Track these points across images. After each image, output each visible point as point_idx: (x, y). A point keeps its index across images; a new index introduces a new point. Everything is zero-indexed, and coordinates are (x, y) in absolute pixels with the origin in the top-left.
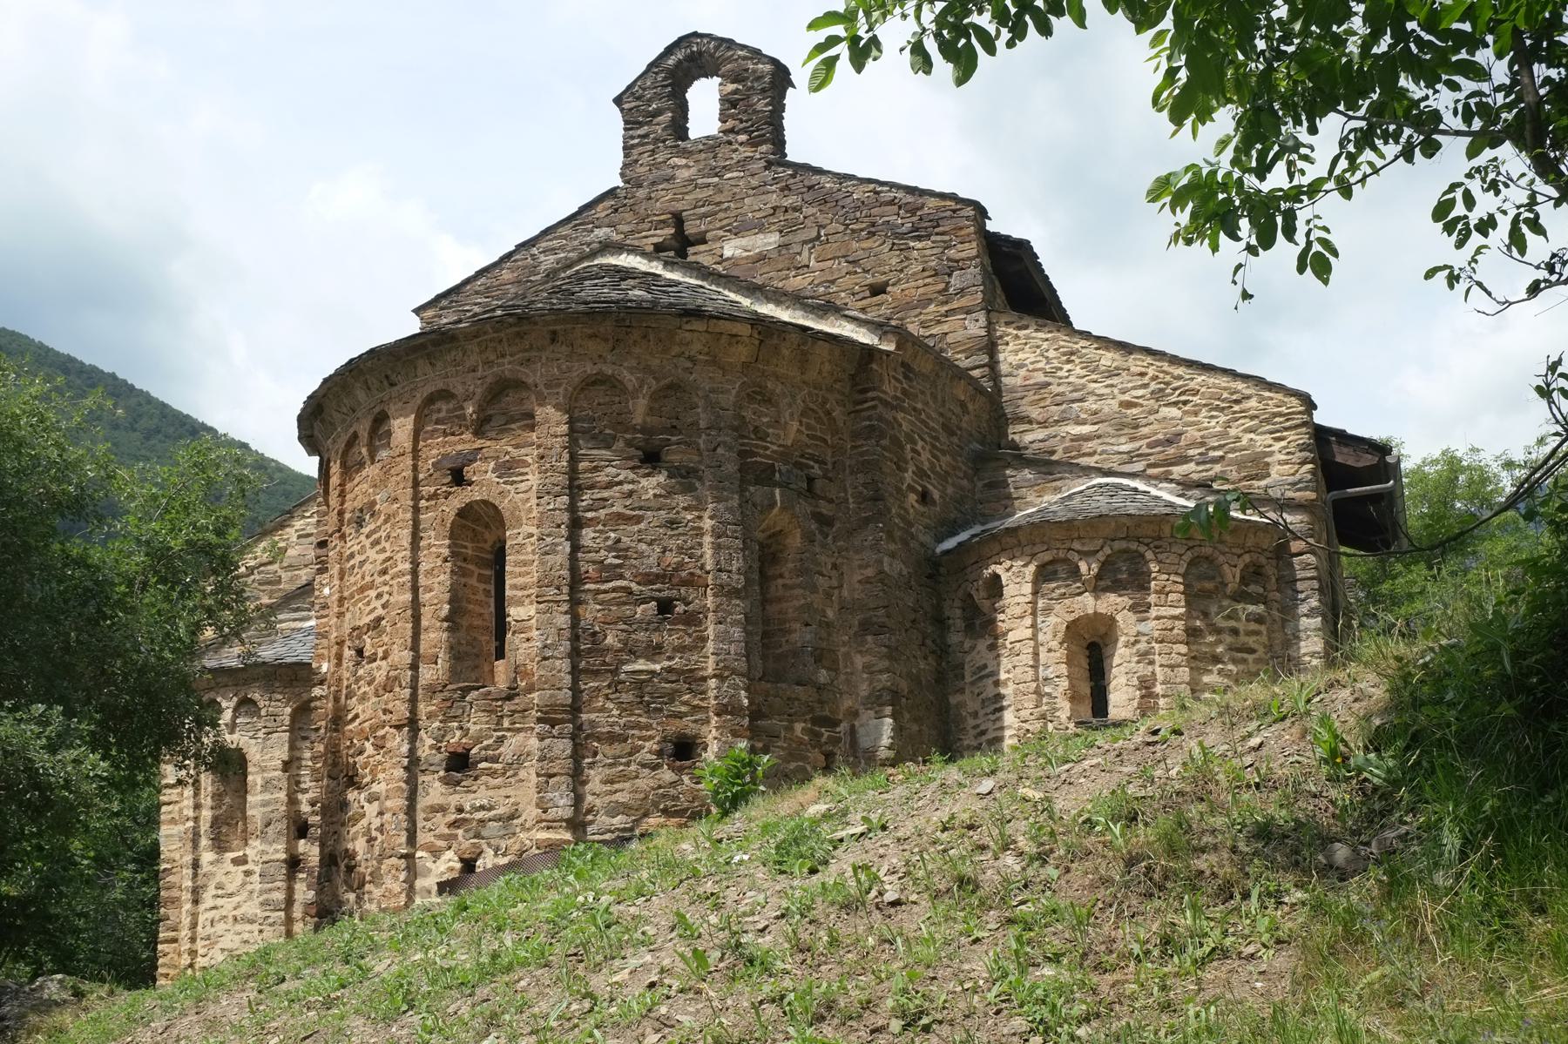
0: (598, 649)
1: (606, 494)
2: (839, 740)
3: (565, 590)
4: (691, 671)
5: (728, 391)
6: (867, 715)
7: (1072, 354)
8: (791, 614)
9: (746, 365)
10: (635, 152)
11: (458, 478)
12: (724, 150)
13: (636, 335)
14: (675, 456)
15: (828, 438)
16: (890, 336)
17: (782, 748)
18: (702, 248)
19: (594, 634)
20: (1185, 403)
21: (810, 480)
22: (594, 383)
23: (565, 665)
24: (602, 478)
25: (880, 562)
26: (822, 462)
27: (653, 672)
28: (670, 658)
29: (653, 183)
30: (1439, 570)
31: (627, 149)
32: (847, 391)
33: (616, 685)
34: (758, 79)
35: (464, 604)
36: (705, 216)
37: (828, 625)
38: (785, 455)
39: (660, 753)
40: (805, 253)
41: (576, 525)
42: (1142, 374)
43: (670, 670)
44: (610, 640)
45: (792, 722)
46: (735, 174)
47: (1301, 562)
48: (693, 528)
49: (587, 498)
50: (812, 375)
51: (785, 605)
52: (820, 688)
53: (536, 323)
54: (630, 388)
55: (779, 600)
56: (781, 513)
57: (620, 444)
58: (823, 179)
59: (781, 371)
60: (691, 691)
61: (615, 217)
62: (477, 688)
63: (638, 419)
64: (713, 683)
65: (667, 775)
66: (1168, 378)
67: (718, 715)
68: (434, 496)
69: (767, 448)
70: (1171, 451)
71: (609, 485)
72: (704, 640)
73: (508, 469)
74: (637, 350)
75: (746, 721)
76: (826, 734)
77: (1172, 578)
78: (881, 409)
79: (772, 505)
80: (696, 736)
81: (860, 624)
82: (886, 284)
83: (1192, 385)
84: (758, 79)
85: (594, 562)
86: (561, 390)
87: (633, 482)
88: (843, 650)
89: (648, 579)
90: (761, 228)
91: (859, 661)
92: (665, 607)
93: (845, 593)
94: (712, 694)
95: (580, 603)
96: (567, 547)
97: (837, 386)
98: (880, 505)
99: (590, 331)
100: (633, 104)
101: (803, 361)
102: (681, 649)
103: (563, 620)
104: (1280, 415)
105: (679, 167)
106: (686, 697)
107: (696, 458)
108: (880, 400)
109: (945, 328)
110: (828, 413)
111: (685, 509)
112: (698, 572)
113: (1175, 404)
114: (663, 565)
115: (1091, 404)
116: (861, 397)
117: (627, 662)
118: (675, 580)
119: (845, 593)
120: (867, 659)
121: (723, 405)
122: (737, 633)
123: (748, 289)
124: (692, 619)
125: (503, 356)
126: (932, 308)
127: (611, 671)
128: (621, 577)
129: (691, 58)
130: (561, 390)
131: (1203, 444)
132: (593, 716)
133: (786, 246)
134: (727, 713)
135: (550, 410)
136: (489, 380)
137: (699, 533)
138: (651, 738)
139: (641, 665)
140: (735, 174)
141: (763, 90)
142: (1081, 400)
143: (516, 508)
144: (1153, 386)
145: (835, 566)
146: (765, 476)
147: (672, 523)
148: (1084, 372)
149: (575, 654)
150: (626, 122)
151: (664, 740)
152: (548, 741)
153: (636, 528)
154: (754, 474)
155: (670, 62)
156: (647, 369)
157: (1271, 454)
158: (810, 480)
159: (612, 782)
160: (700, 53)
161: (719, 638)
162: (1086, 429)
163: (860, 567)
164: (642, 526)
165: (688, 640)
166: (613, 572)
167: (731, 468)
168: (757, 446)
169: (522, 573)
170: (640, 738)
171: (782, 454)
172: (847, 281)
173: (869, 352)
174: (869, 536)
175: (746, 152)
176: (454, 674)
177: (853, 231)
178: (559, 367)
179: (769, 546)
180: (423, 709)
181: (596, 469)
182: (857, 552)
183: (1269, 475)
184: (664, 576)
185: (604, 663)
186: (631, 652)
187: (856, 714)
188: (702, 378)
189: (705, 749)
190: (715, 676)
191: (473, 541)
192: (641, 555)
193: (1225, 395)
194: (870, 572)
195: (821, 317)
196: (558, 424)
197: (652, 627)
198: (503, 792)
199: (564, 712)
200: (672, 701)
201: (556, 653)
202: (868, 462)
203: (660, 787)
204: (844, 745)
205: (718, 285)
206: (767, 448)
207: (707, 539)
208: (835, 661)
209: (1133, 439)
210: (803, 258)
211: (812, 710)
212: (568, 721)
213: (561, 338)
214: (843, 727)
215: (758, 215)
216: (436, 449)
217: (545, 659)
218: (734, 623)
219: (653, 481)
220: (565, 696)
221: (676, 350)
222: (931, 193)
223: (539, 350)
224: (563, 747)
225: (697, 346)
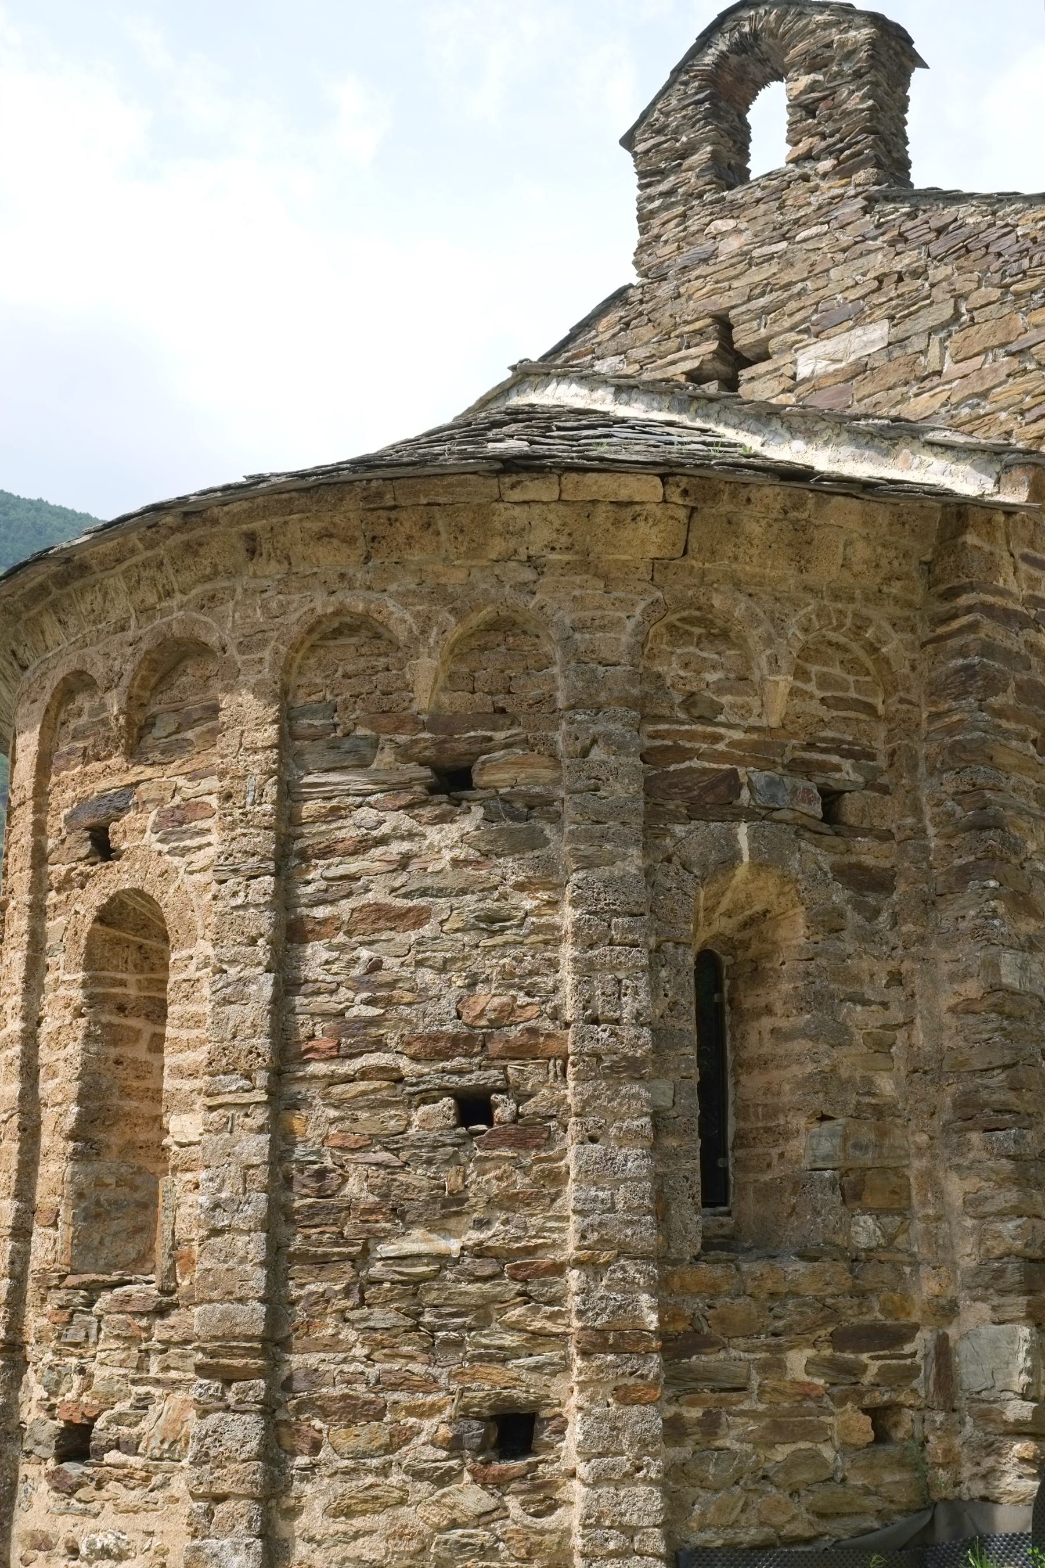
0: (330, 1208)
1: (352, 866)
2: (912, 1372)
3: (261, 1078)
4: (530, 1251)
6: (975, 1314)
8: (789, 1096)
10: (656, 222)
11: (103, 849)
12: (798, 190)
13: (408, 523)
14: (498, 774)
15: (878, 701)
16: (1018, 474)
17: (753, 1415)
18: (762, 367)
19: (321, 1174)
21: (831, 798)
22: (337, 633)
23: (252, 1246)
24: (348, 831)
25: (993, 966)
26: (860, 755)
27: (442, 1259)
28: (481, 1224)
29: (684, 269)
31: (644, 218)
32: (917, 598)
33: (362, 1290)
34: (849, 56)
35: (115, 1101)
36: (766, 311)
37: (879, 1111)
38: (763, 749)
39: (454, 1445)
40: (935, 350)
41: (291, 934)
43: (481, 1252)
44: (353, 1187)
45: (779, 1349)
46: (814, 230)
48: (537, 929)
49: (317, 874)
50: (826, 571)
51: (775, 1075)
52: (855, 1260)
53: (215, 522)
54: (402, 636)
55: (764, 1063)
56: (754, 877)
57: (385, 757)
58: (962, 210)
59: (747, 569)
61: (626, 338)
62: (112, 1286)
63: (422, 702)
64: (574, 1278)
65: (471, 1497)
67: (585, 1354)
68: (65, 884)
69: (717, 738)
71: (362, 847)
72: (557, 1178)
73: (177, 821)
74: (415, 556)
75: (653, 1366)
76: (874, 1367)
78: (989, 628)
79: (730, 860)
80: (539, 1403)
81: (957, 1106)
84: (849, 56)
85: (325, 1015)
86: (267, 654)
87: (410, 836)
88: (918, 1164)
89: (435, 1048)
90: (859, 318)
91: (956, 1188)
92: (473, 1108)
93: (920, 1038)
94: (573, 1302)
95: (295, 1105)
96: (265, 987)
97: (895, 588)
98: (992, 839)
99: (315, 526)
100: (651, 144)
101: (800, 543)
102: (508, 1202)
103: (254, 1147)
105: (723, 234)
106: (515, 1314)
107: (547, 774)
108: (988, 610)
110: (872, 649)
111: (520, 887)
112: (547, 1025)
114: (468, 1015)
116: (947, 606)
117: (385, 1236)
118: (495, 1047)
119: (920, 1038)
120: (972, 1184)
121: (605, 653)
122: (633, 1160)
123: (757, 417)
124: (533, 1133)
125: (169, 594)
127: (352, 1259)
128: (379, 1045)
129: (741, 47)
130: (267, 654)
132: (313, 1359)
133: (900, 342)
134: (605, 1348)
135: (247, 698)
136: (144, 646)
137: (552, 937)
138: (435, 1409)
139: (417, 1241)
140: (814, 230)
141: (858, 75)
143: (187, 904)
145: (896, 979)
146: (718, 798)
147: (491, 918)
149: (278, 1220)
150: (642, 175)
151: (465, 1413)
152: (213, 1419)
153: (413, 936)
154: (680, 793)
155: (708, 59)
156: (440, 594)
158: (831, 798)
159: (349, 1513)
160: (755, 34)
161: (589, 1175)
163: (953, 977)
164: (427, 930)
165: (521, 1182)
166: (358, 1037)
167: (623, 790)
168: (691, 736)
169: (187, 1048)
170: (411, 1411)
171: (755, 747)
172: (1012, 390)
173: (958, 511)
174: (965, 909)
175: (832, 188)
176: (83, 1247)
177: (1018, 295)
178: (264, 607)
179: (745, 945)
180: (35, 1321)
181: (335, 813)
182: (947, 943)
184: (470, 1039)
185: (340, 1239)
186: (397, 1213)
187: (949, 1311)
188: (556, 602)
189: (561, 1431)
190: (578, 1263)
191: (138, 968)
192: (422, 994)
194: (972, 989)
195: (886, 454)
196: (259, 725)
197: (440, 1154)
198: (143, 1521)
199: (249, 1352)
200: (483, 1321)
201: (238, 1221)
202: (962, 746)
203: (454, 1524)
204: (923, 1385)
205: (707, 417)
206: (717, 738)
207: (567, 951)
208: (902, 1192)
210: (931, 361)
211: (834, 1314)
212: (260, 1373)
213: (266, 547)
214: (922, 1342)
215: (852, 295)
216: (75, 786)
217: (216, 1232)
218: (628, 1137)
219: (453, 831)
220: (252, 1317)
221: (497, 547)
223: (230, 575)
224: (244, 1431)
225: (540, 537)
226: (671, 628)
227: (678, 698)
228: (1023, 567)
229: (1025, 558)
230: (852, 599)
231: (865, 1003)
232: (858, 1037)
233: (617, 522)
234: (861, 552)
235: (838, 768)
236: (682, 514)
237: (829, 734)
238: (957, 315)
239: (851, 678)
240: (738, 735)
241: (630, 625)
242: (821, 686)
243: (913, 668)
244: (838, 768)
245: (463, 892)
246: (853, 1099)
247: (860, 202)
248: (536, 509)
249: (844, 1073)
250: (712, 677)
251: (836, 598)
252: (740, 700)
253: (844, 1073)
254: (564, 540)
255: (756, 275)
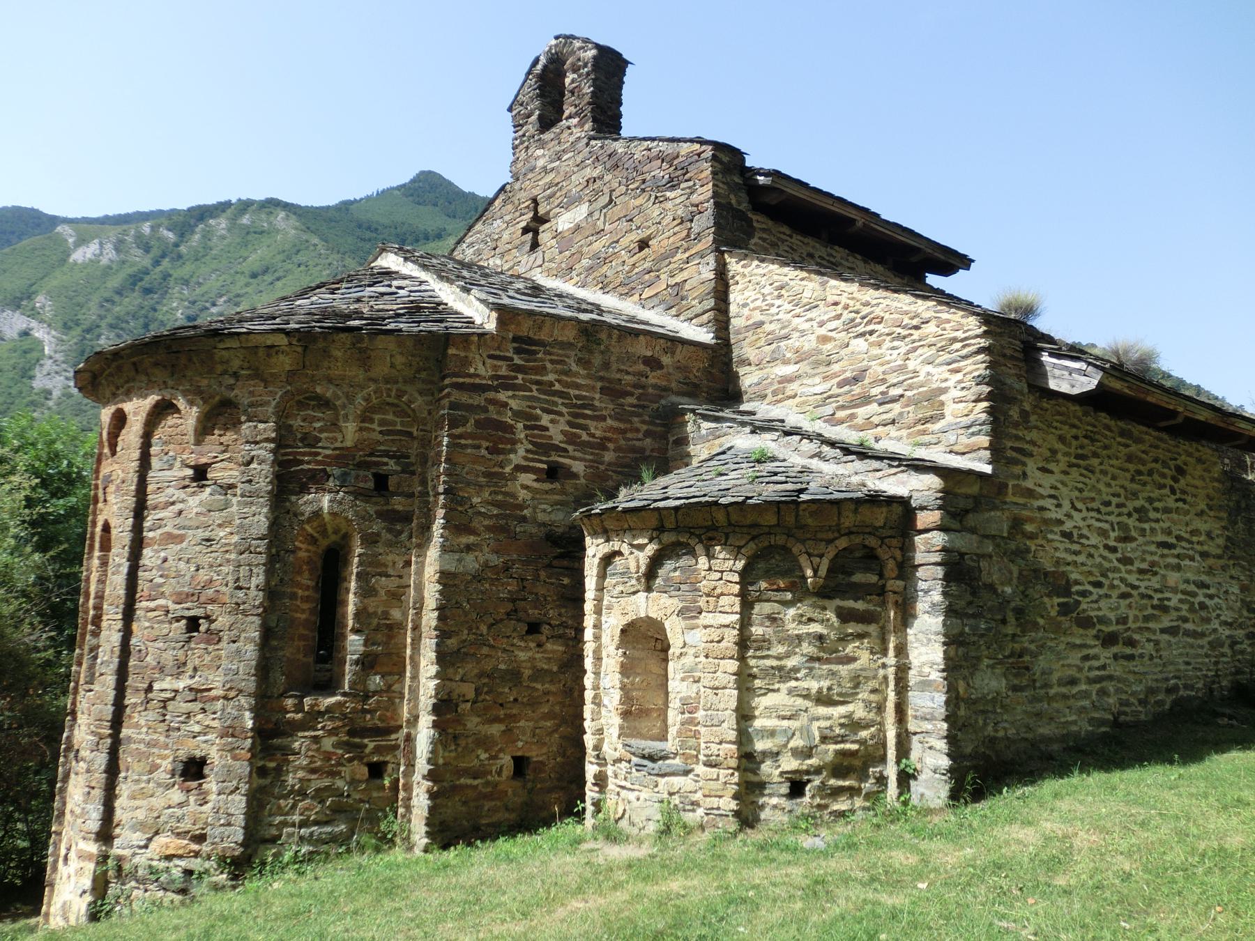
5: (268, 403)
7: (782, 288)
9: (291, 374)
13: (183, 361)
20: (871, 333)
30: (350, 760)
42: (836, 304)
47: (926, 542)
50: (381, 370)
60: (204, 710)
65: (176, 795)
66: (858, 306)
69: (318, 454)
70: (857, 389)
74: (189, 373)
76: (371, 745)
77: (726, 576)
82: (649, 238)
83: (878, 311)
87: (183, 501)
92: (193, 624)
97: (423, 375)
104: (955, 340)
109: (685, 275)
111: (220, 526)
113: (862, 335)
115: (795, 342)
118: (202, 599)
126: (679, 256)
128: (162, 595)
131: (884, 381)
142: (787, 337)
144: (847, 316)
147: (208, 540)
148: (790, 307)
153: (179, 547)
157: (944, 391)
162: (789, 370)
164: (184, 545)
171: (337, 457)
183: (942, 416)
186: (161, 670)
193: (906, 321)
203: (169, 807)
206: (318, 454)
209: (826, 378)
221: (219, 369)
222: (685, 141)
225: (236, 363)
226: (299, 402)
227: (299, 436)
228: (489, 361)
229: (490, 357)
230: (397, 382)
231: (388, 576)
232: (382, 592)
233: (269, 356)
234: (399, 360)
235: (386, 464)
236: (299, 349)
237: (382, 448)
238: (611, 201)
239: (398, 420)
240: (328, 452)
241: (274, 403)
242: (380, 425)
243: (430, 413)
244: (386, 464)
245: (198, 528)
246: (375, 621)
247: (585, 140)
248: (232, 352)
249: (371, 610)
250: (318, 425)
251: (387, 382)
252: (331, 435)
253: (371, 610)
254: (246, 365)
255: (548, 178)
